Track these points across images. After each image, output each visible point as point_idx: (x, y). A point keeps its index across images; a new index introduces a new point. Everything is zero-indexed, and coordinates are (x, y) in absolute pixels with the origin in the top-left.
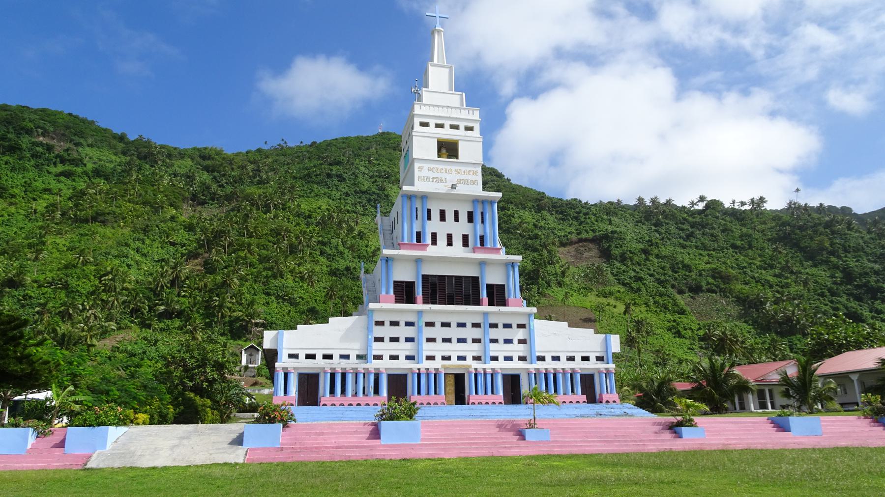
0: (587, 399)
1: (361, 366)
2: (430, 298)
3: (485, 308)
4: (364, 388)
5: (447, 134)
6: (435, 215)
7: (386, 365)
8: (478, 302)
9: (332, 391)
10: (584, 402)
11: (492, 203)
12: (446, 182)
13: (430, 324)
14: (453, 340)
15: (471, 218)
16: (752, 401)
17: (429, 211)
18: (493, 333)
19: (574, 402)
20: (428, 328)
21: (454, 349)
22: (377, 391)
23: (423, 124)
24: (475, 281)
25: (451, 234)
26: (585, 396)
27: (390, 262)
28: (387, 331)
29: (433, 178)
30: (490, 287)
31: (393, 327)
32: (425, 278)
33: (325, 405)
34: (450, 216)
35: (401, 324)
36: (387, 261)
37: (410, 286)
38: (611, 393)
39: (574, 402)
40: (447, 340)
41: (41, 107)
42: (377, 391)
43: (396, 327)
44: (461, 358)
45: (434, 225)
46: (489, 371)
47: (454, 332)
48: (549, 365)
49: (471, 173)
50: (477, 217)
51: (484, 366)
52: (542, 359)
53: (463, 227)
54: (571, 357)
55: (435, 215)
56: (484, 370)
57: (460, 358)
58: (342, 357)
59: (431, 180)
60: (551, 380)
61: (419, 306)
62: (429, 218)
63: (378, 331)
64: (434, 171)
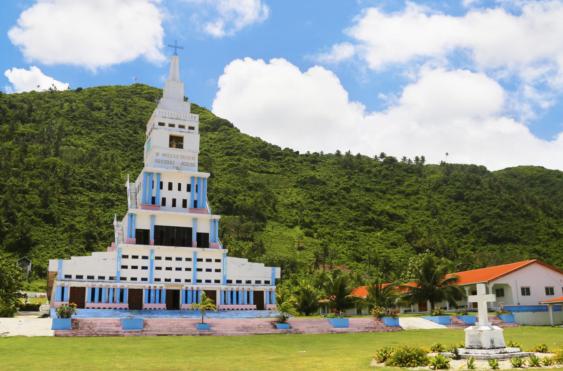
0: (166, 307)
1: (112, 285)
2: (159, 241)
3: (195, 249)
4: (113, 298)
5: (176, 132)
6: (166, 186)
7: (128, 285)
8: (190, 245)
9: (93, 300)
10: (255, 309)
11: (204, 179)
12: (174, 164)
13: (158, 258)
14: (172, 269)
15: (189, 188)
16: (321, 310)
17: (161, 183)
18: (200, 265)
19: (240, 309)
20: (157, 260)
21: (173, 274)
22: (121, 300)
23: (192, 128)
24: (189, 231)
25: (175, 199)
26: (256, 306)
27: (134, 217)
28: (130, 262)
29: (165, 161)
30: (199, 235)
31: (187, 262)
32: (157, 228)
33: (88, 308)
34: (175, 187)
35: (139, 258)
36: (132, 216)
37: (147, 232)
38: (160, 302)
39: (240, 309)
40: (169, 269)
41: (505, 168)
42: (121, 300)
43: (136, 260)
44: (178, 280)
45: (184, 194)
46: (152, 288)
47: (174, 264)
48: (234, 287)
49: (191, 158)
50: (193, 188)
51: (150, 285)
52: (229, 282)
53: (184, 194)
54: (249, 281)
55: (166, 186)
56: (192, 288)
57: (177, 280)
58: (166, 280)
59: (164, 162)
60: (234, 297)
61: (152, 247)
62: (161, 188)
63: (125, 262)
64: (167, 156)
